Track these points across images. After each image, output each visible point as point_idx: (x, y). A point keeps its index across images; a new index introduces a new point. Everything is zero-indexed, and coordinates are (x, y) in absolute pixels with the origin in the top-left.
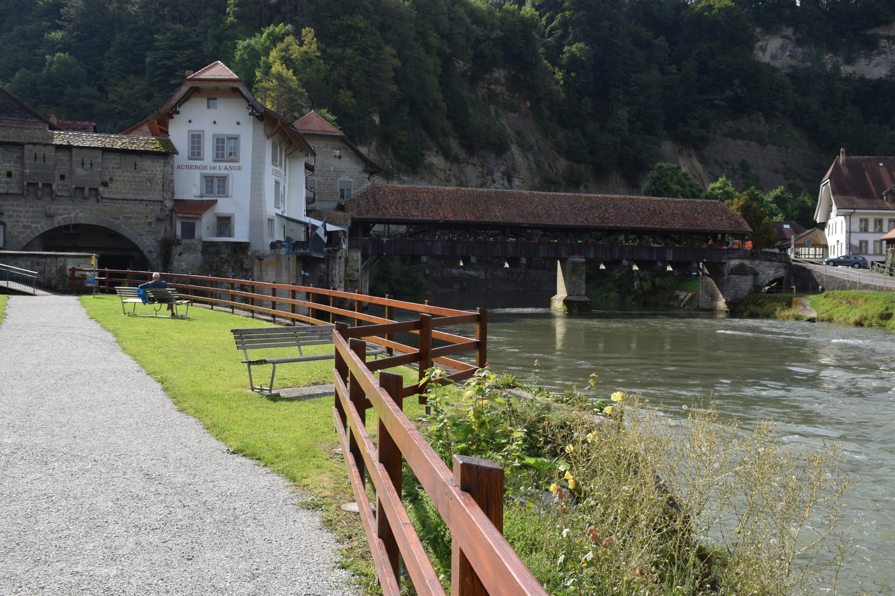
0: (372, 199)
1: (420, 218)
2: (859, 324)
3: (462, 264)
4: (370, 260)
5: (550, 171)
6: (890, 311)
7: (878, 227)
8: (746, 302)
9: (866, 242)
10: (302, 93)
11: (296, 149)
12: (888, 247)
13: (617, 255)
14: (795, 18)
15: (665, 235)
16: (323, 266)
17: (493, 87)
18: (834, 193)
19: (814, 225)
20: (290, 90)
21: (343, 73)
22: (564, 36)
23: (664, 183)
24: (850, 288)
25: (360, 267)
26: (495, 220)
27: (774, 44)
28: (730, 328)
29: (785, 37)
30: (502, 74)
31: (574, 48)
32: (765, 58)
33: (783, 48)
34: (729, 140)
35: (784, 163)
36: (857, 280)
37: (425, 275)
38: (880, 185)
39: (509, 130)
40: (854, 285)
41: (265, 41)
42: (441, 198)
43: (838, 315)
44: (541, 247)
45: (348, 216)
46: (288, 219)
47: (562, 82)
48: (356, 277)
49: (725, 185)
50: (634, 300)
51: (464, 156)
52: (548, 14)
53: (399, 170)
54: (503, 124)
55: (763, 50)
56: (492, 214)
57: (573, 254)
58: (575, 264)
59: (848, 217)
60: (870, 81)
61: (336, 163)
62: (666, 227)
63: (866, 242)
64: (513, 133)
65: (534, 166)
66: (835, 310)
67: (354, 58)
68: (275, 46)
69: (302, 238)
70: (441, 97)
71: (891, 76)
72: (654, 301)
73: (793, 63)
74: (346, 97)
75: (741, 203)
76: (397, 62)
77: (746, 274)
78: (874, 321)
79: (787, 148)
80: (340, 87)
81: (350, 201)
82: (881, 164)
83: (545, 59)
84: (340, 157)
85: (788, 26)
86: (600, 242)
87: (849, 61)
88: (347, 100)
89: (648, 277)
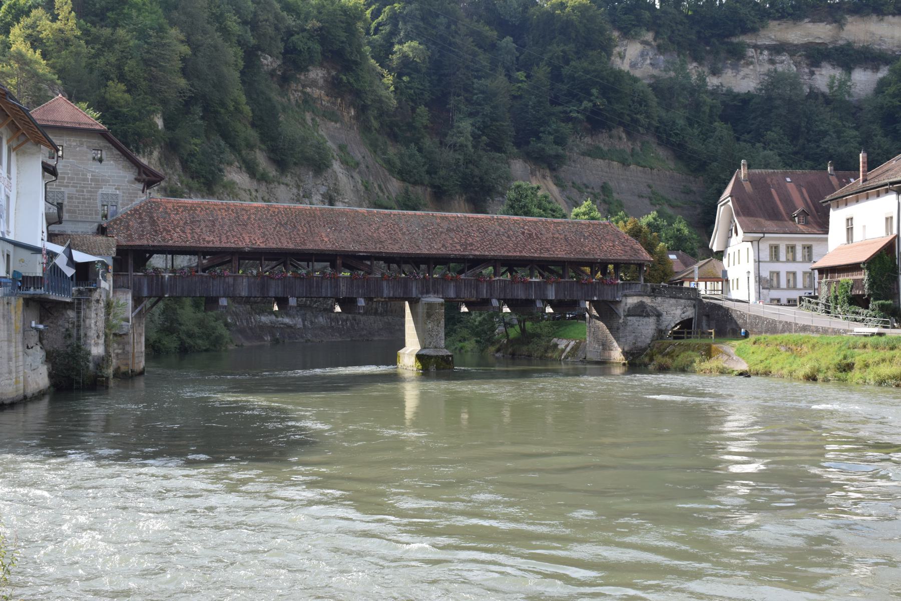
0: (147, 219)
1: (217, 245)
2: (812, 378)
3: (276, 308)
4: (147, 303)
5: (381, 194)
6: (849, 361)
7: (790, 254)
8: (648, 351)
9: (778, 274)
10: (52, 80)
11: (27, 140)
12: (821, 278)
13: (484, 294)
14: (655, 22)
15: (543, 265)
16: (71, 314)
17: (308, 90)
18: (738, 215)
19: (710, 253)
20: (34, 75)
21: (113, 60)
22: (393, 33)
23: (524, 206)
24: (783, 331)
25: (129, 314)
26: (322, 247)
27: (633, 50)
28: (619, 383)
29: (645, 43)
30: (320, 75)
31: (406, 47)
32: (625, 67)
33: (643, 55)
34: (588, 159)
35: (649, 187)
36: (793, 321)
37: (226, 325)
38: (791, 207)
39: (330, 144)
40: (787, 327)
41: (5, 16)
42: (246, 217)
43: (779, 366)
44: (385, 283)
45: (111, 244)
46: (16, 244)
47: (392, 88)
48: (125, 330)
49: (591, 210)
50: (498, 351)
51: (274, 173)
52: (373, 7)
53: (190, 189)
54: (322, 136)
55: (622, 57)
56: (317, 239)
57: (428, 292)
58: (430, 306)
59: (755, 243)
60: (738, 94)
61: (95, 167)
62: (546, 255)
63: (794, 274)
64: (334, 147)
65: (361, 187)
66: (773, 360)
67: (128, 41)
68: (18, 22)
69: (39, 272)
70: (243, 99)
71: (761, 90)
72: (523, 354)
73: (656, 72)
74: (117, 91)
75: (629, 227)
76: (185, 49)
77: (648, 316)
78: (830, 373)
79: (652, 169)
80: (108, 78)
81: (115, 221)
82: (788, 180)
83: (373, 57)
84: (100, 160)
85: (648, 30)
86: (462, 276)
87: (715, 72)
88: (119, 95)
89: (516, 322)
